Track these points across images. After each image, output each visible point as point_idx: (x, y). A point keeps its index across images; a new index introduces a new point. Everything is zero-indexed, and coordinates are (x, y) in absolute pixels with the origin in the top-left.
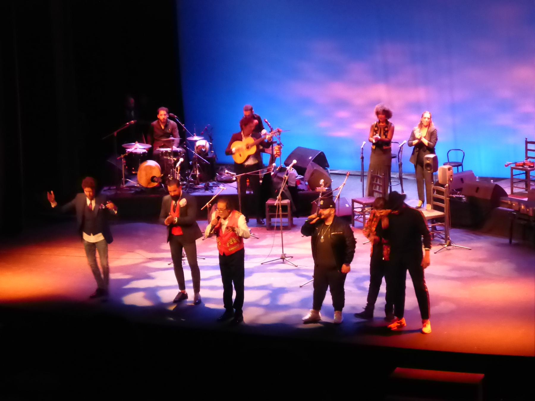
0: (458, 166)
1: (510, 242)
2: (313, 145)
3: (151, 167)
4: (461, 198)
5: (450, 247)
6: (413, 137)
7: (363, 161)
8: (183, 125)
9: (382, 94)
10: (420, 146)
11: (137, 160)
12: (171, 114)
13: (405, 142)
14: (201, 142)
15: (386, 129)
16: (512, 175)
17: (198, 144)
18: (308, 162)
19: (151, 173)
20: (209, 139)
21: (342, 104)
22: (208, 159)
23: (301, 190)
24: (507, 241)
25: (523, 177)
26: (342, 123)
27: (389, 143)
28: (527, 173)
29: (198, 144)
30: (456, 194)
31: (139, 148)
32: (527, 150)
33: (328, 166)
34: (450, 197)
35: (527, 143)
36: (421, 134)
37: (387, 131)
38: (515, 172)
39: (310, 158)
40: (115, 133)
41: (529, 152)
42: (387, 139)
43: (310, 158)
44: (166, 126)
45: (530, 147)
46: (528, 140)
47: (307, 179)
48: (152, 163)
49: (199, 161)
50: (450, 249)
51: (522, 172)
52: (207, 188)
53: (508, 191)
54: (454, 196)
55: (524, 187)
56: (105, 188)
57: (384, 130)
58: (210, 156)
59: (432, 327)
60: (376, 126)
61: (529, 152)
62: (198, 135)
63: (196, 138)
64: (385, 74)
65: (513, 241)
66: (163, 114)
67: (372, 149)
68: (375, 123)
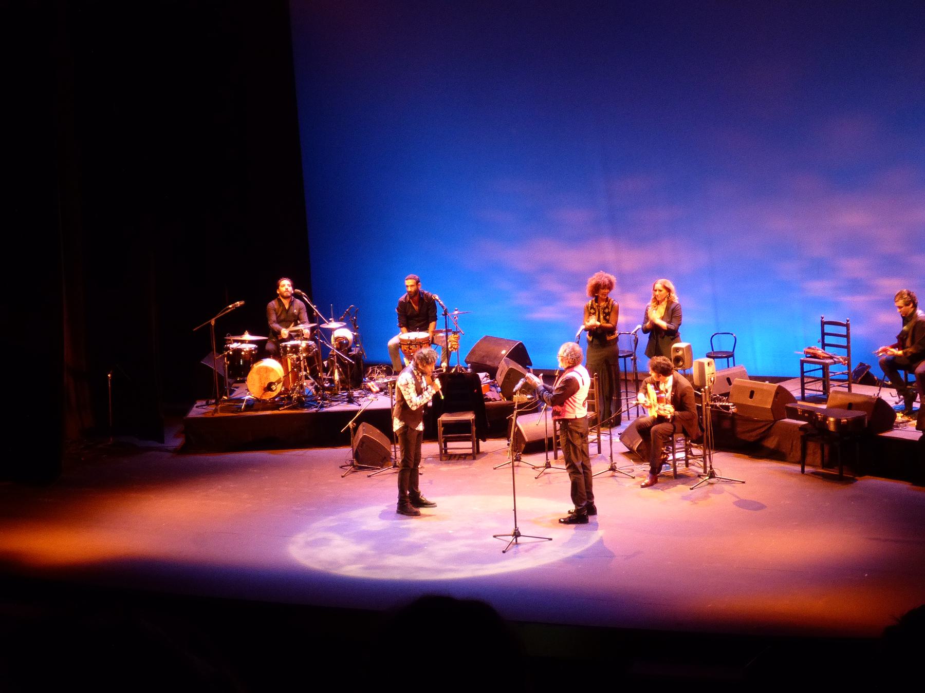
0: (728, 357)
1: (803, 471)
2: (509, 333)
3: (268, 370)
4: (727, 408)
5: (712, 480)
6: (647, 318)
7: (635, 363)
8: (314, 307)
9: (605, 259)
10: (654, 331)
11: (241, 367)
12: (297, 290)
13: (640, 326)
14: (341, 332)
15: (607, 311)
16: (803, 372)
17: (337, 334)
18: (498, 358)
19: (267, 378)
20: (351, 326)
21: (548, 269)
22: (352, 357)
23: (490, 400)
24: (798, 468)
25: (819, 374)
26: (549, 299)
27: (612, 331)
28: (825, 368)
29: (337, 334)
30: (720, 400)
31: (246, 342)
32: (824, 334)
33: (531, 364)
34: (712, 406)
35: (823, 324)
36: (657, 316)
37: (609, 314)
38: (807, 367)
39: (504, 352)
40: (213, 322)
41: (845, 333)
42: (609, 325)
43: (504, 352)
44: (291, 303)
45: (828, 329)
46: (825, 320)
47: (500, 384)
48: (270, 363)
49: (339, 359)
50: (712, 484)
51: (818, 366)
52: (351, 400)
53: (797, 394)
54: (718, 404)
55: (821, 389)
56: (199, 403)
57: (604, 312)
58: (355, 351)
59: (191, 404)
60: (592, 308)
61: (845, 333)
62: (337, 320)
63: (333, 325)
64: (616, 224)
65: (807, 469)
66: (285, 285)
67: (588, 341)
68: (590, 303)
